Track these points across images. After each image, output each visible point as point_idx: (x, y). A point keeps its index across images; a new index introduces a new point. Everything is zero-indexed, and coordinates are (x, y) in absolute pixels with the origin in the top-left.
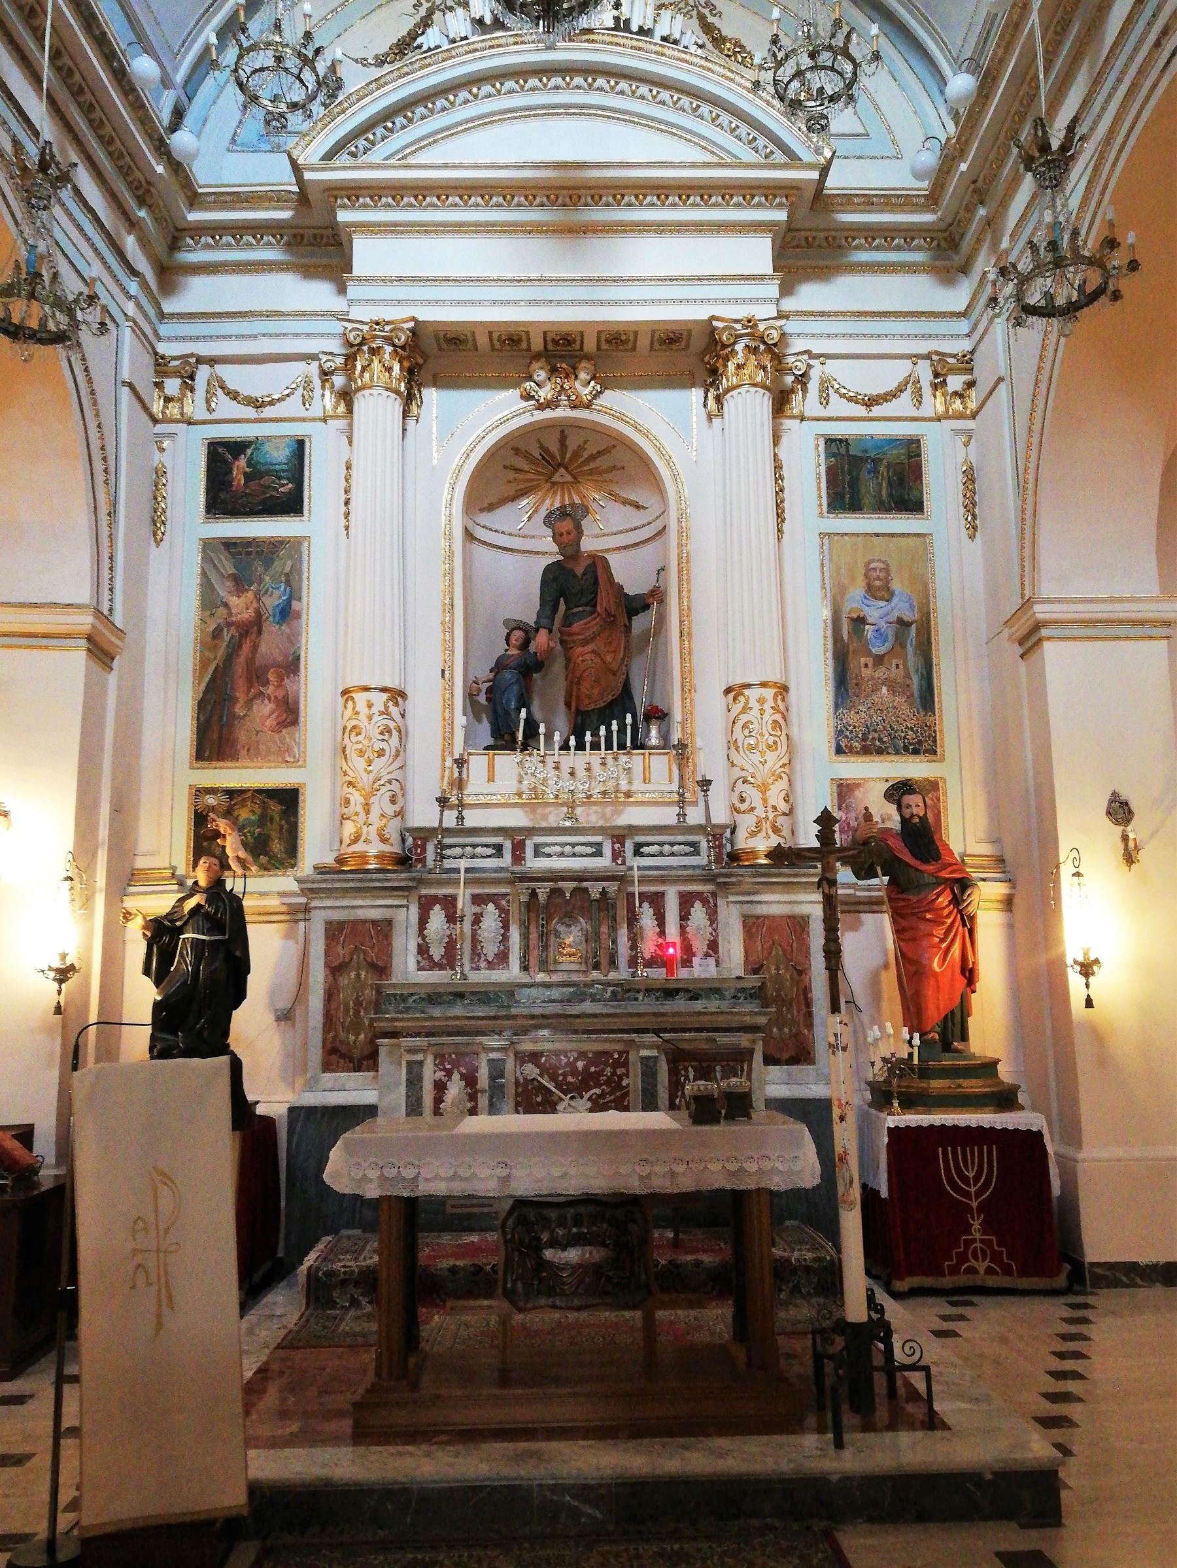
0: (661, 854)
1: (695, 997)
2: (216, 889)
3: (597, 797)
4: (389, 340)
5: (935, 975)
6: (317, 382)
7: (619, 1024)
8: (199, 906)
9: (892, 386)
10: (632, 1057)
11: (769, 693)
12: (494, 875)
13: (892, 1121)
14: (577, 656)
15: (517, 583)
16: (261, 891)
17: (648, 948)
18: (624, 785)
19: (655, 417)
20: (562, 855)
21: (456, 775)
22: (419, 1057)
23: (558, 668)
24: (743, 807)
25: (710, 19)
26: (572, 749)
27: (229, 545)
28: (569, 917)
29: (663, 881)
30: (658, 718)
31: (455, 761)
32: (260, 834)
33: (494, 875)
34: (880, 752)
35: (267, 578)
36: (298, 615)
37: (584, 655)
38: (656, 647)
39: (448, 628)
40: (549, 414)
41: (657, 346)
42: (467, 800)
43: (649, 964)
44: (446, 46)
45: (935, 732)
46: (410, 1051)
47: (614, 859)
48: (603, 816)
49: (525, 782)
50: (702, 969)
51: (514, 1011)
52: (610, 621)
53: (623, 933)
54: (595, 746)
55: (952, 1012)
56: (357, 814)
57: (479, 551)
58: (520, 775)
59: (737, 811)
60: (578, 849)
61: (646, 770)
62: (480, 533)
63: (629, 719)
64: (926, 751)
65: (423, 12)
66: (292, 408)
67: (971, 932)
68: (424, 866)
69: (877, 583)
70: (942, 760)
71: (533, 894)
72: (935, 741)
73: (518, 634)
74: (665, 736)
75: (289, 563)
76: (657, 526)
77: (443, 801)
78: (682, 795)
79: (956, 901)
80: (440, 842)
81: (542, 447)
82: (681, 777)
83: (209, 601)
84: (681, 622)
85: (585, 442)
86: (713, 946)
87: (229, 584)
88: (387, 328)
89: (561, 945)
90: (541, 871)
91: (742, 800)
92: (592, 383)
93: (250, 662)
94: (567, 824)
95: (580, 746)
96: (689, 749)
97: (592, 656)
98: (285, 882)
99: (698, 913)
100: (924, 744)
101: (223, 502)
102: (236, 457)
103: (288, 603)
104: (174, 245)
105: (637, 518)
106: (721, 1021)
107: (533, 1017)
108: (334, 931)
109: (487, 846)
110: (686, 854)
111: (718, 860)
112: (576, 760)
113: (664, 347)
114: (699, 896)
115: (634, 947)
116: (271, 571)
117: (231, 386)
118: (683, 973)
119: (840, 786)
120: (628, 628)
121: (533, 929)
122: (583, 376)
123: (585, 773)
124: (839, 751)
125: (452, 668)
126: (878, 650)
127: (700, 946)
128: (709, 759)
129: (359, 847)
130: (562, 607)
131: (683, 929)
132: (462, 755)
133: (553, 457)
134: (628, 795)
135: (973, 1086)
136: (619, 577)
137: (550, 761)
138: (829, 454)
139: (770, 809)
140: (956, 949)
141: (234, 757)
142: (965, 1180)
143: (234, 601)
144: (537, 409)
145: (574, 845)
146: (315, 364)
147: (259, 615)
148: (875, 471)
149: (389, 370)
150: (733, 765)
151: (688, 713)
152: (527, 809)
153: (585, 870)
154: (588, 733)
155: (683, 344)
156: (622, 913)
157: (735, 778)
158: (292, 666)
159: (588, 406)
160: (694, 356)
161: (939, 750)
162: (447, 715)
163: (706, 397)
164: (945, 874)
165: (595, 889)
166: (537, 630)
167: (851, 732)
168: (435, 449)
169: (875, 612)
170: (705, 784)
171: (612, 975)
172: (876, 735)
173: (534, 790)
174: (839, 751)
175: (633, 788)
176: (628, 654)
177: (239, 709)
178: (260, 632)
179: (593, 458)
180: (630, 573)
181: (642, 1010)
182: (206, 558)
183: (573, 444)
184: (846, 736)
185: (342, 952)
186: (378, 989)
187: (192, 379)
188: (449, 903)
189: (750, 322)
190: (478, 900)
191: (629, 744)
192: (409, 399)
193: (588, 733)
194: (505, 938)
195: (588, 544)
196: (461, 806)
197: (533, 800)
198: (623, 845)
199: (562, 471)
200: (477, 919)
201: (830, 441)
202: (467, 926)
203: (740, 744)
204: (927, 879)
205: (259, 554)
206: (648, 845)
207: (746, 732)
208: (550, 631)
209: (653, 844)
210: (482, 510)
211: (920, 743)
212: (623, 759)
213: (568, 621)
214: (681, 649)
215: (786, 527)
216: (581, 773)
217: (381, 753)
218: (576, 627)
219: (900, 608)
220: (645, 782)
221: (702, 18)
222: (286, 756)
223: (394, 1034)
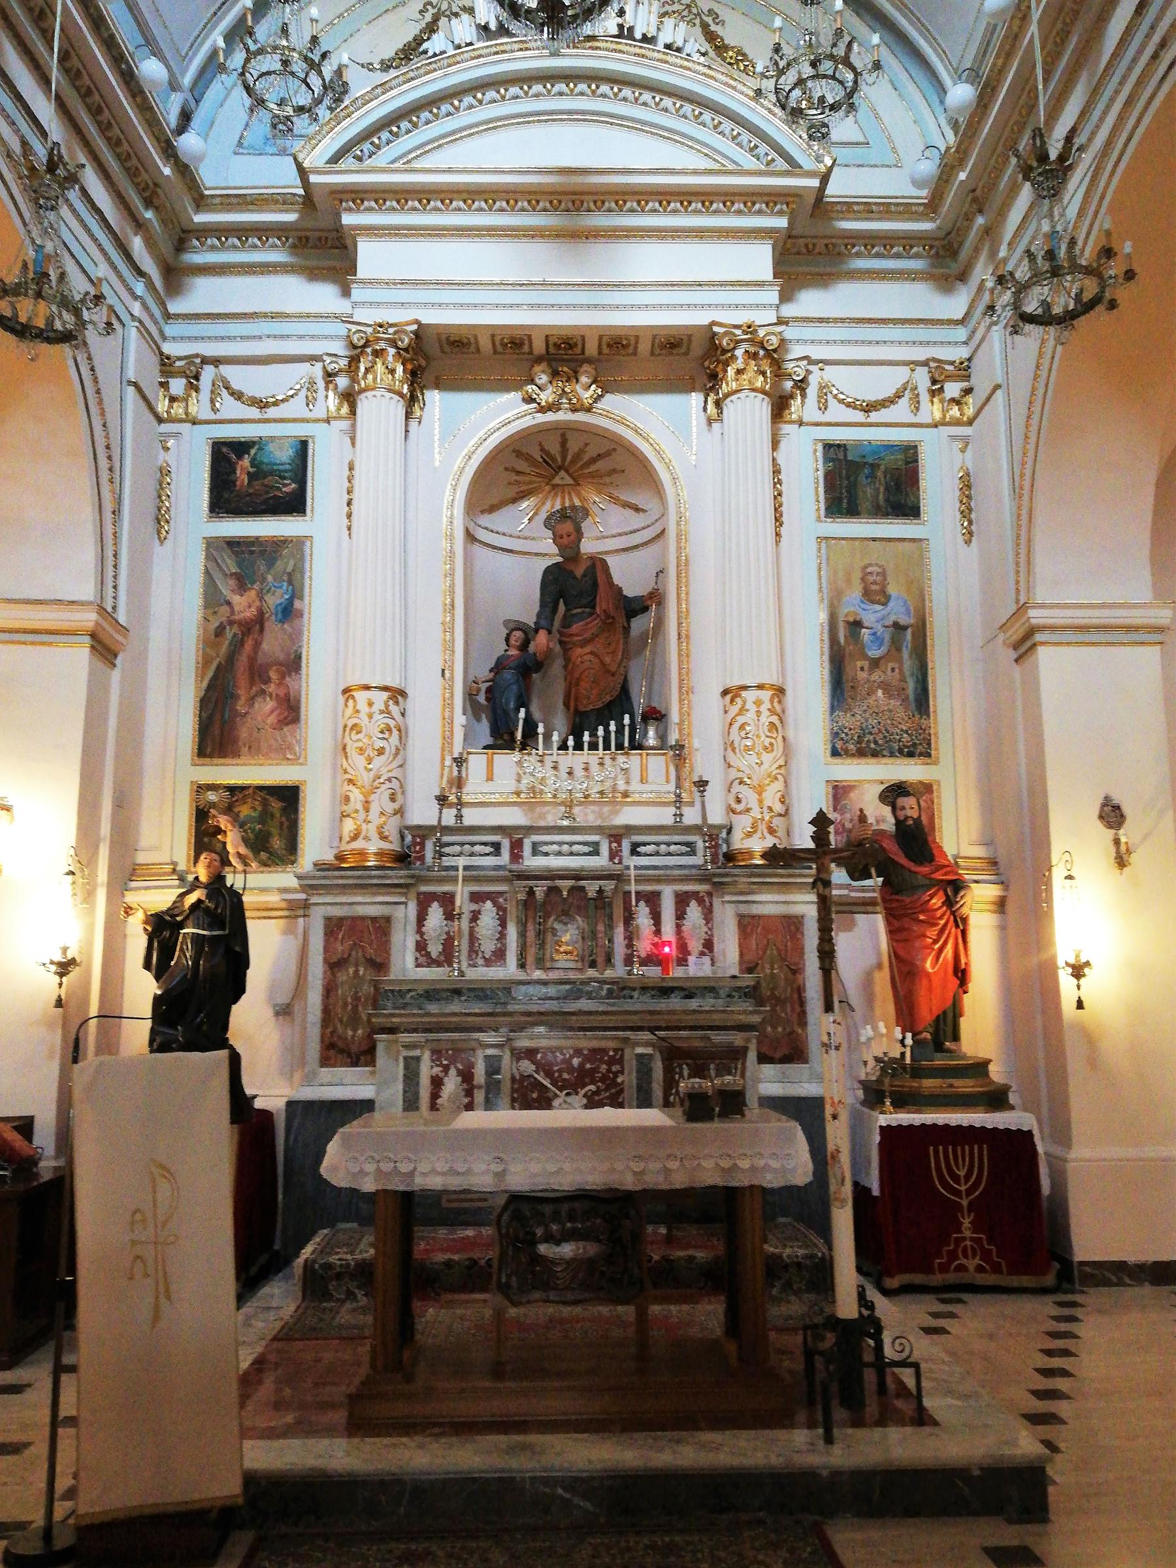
0: (657, 854)
1: (690, 996)
2: (217, 886)
3: (595, 796)
4: (393, 343)
5: (928, 975)
6: (321, 384)
7: (611, 1021)
8: (199, 901)
9: (889, 392)
10: (628, 1053)
11: (766, 695)
13: (883, 1120)
14: (576, 656)
15: (517, 585)
16: (261, 887)
17: (644, 946)
18: (622, 786)
19: (657, 421)
20: (559, 854)
21: (456, 773)
22: (417, 1053)
25: (713, 28)
26: (571, 749)
27: (234, 544)
28: (565, 915)
29: (658, 880)
30: (656, 719)
31: (455, 760)
32: (260, 830)
34: (875, 754)
35: (270, 578)
36: (300, 615)
37: (580, 654)
38: (654, 653)
39: (449, 628)
40: (550, 417)
42: (465, 799)
43: (644, 962)
44: (451, 52)
45: (930, 735)
46: (407, 1047)
47: (611, 858)
50: (697, 968)
51: (510, 1008)
52: (608, 623)
53: (619, 932)
54: (593, 746)
55: (944, 1012)
56: (357, 811)
57: (477, 549)
59: (734, 812)
61: (644, 769)
62: (482, 535)
63: (627, 720)
64: (921, 754)
65: (428, 17)
66: (296, 408)
67: (964, 933)
68: (423, 863)
69: (874, 587)
70: (936, 763)
71: (531, 892)
72: (929, 744)
73: (518, 634)
74: (662, 737)
75: (292, 563)
77: (442, 800)
78: (679, 796)
79: (949, 903)
80: (439, 840)
81: (542, 450)
82: (678, 778)
83: (212, 599)
84: (679, 624)
86: (708, 945)
87: (232, 582)
88: (391, 330)
89: (559, 943)
90: (538, 869)
91: (739, 801)
92: (593, 387)
93: (252, 660)
94: (565, 823)
95: (579, 746)
96: (686, 751)
98: (285, 878)
99: (694, 912)
100: (919, 747)
101: (228, 501)
102: (240, 457)
103: (290, 602)
104: (181, 246)
105: (637, 521)
106: (717, 1019)
107: (529, 1014)
108: (333, 927)
110: (682, 854)
111: (714, 861)
112: (574, 759)
114: (695, 895)
115: (630, 946)
116: (272, 571)
117: (235, 386)
118: (677, 972)
119: (835, 787)
120: (627, 630)
121: (530, 926)
122: (584, 379)
123: (583, 773)
124: (835, 753)
126: (874, 653)
127: (695, 946)
128: (706, 761)
129: (358, 844)
130: (562, 607)
131: (678, 927)
132: (461, 754)
133: (554, 459)
134: (626, 795)
135: (965, 1085)
137: (548, 761)
138: (827, 459)
139: (765, 810)
140: (949, 950)
141: (236, 754)
142: (956, 1179)
143: (236, 599)
145: (571, 844)
146: (319, 365)
147: (261, 612)
148: (872, 476)
149: (392, 372)
150: (729, 766)
151: (685, 715)
153: (582, 869)
154: (586, 733)
156: (618, 912)
158: (293, 664)
159: (589, 410)
160: (694, 361)
161: (933, 752)
163: (706, 402)
164: (939, 876)
165: (592, 888)
166: (536, 631)
167: (847, 734)
168: (437, 450)
169: (871, 616)
170: (702, 784)
171: (609, 973)
172: (871, 738)
173: (532, 789)
174: (835, 753)
175: (631, 788)
176: (627, 656)
177: (241, 707)
178: (262, 630)
179: (593, 460)
180: (630, 576)
181: (638, 1007)
182: (209, 557)
183: (573, 446)
184: (842, 739)
185: (340, 948)
186: (376, 984)
187: (197, 379)
188: (447, 900)
189: (750, 328)
190: (476, 897)
192: (412, 401)
193: (586, 733)
194: (502, 936)
195: (588, 546)
196: (460, 804)
197: (531, 799)
198: (620, 845)
199: (562, 473)
200: (475, 917)
201: (828, 446)
202: (465, 924)
203: (736, 744)
204: (922, 881)
205: (262, 553)
206: (645, 844)
207: (743, 734)
208: (550, 632)
210: (483, 512)
211: (914, 745)
212: (621, 759)
213: (567, 622)
215: (783, 530)
216: (579, 773)
217: (381, 752)
218: (575, 628)
219: (896, 611)
220: (642, 781)
221: (705, 26)
222: (287, 753)
223: (392, 1030)
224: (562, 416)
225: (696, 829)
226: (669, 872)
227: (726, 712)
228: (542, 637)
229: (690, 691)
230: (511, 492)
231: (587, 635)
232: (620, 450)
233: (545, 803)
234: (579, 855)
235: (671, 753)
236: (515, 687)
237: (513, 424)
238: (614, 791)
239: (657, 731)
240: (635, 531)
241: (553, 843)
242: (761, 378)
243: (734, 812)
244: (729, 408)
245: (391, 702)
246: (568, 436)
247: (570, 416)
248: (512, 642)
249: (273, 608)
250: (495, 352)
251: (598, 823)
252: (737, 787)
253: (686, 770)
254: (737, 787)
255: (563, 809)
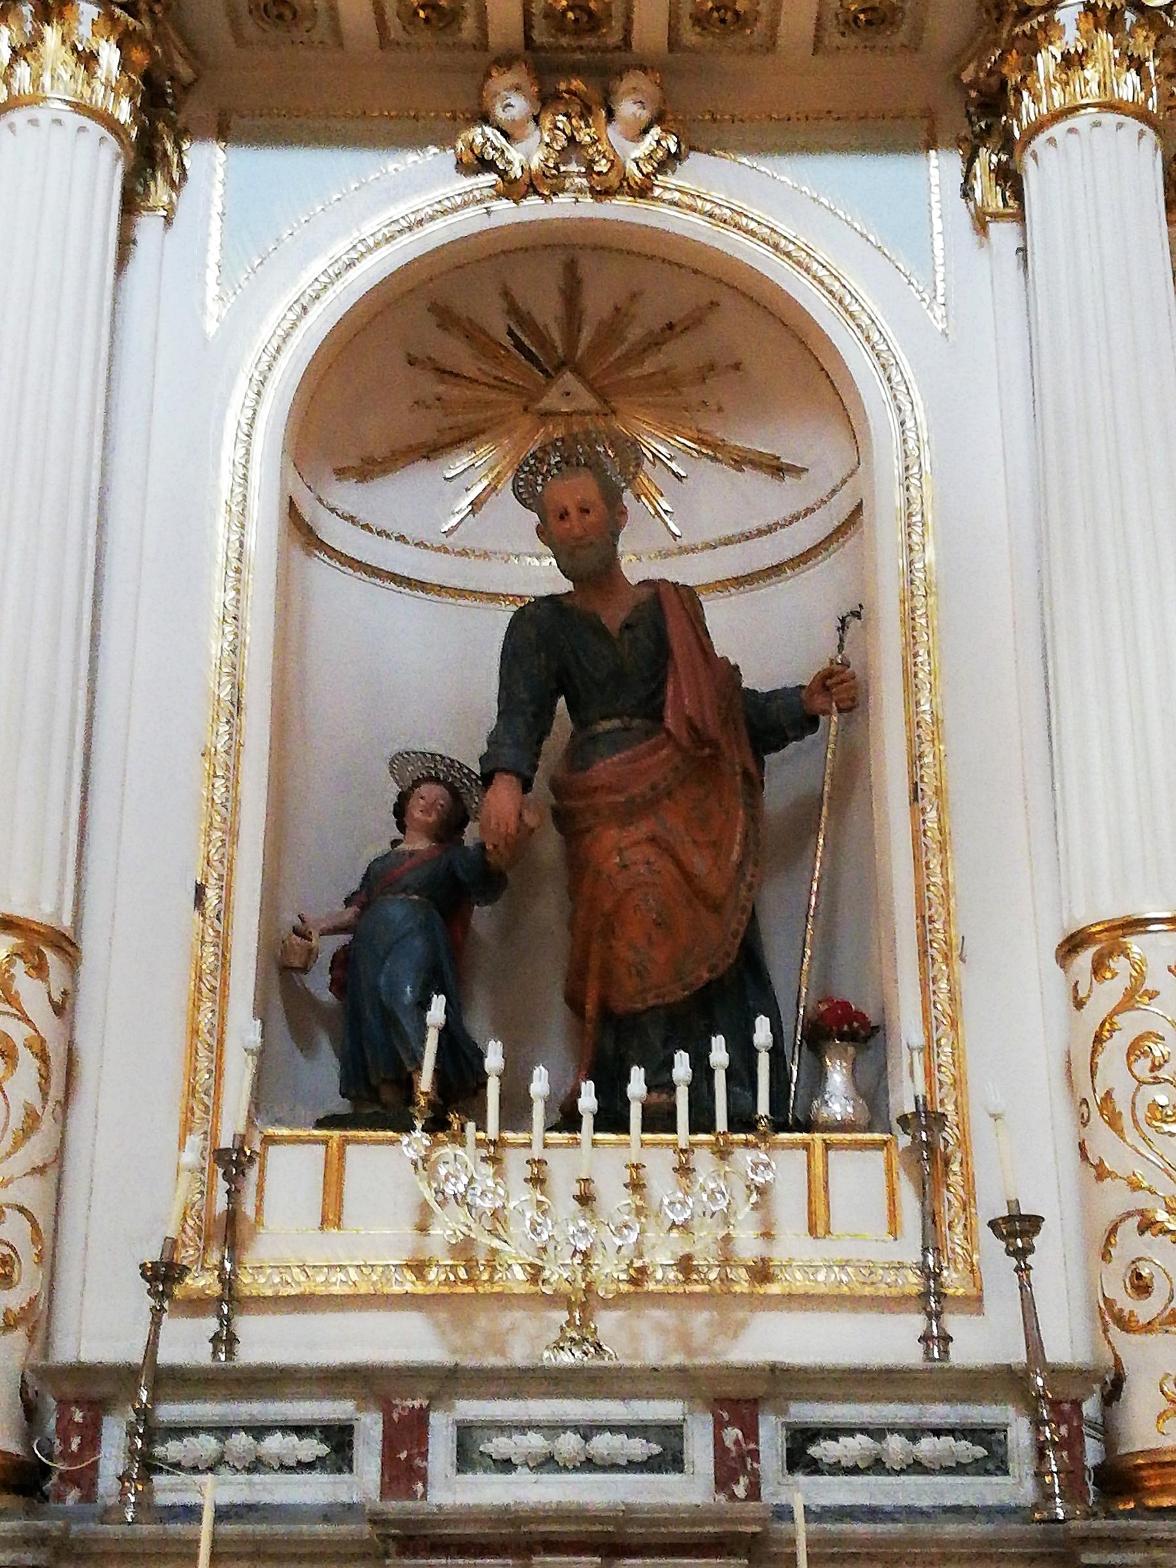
0: (877, 1466)
3: (663, 1276)
12: (321, 1529)
15: (432, 674)
18: (748, 1246)
20: (548, 1463)
21: (221, 1204)
23: (548, 909)
24: (1146, 1309)
26: (588, 1123)
30: (851, 1037)
31: (220, 1156)
33: (321, 1529)
37: (621, 849)
38: (834, 849)
40: (533, 209)
41: (833, 38)
42: (250, 1283)
47: (724, 1480)
48: (685, 1341)
49: (435, 1231)
52: (701, 761)
54: (659, 1119)
57: (322, 575)
58: (425, 1209)
59: (1125, 1323)
60: (603, 1444)
62: (334, 531)
68: (89, 1495)
73: (431, 792)
74: (872, 1094)
76: (840, 508)
77: (163, 1276)
78: (931, 1275)
80: (144, 1414)
81: (513, 310)
82: (931, 1219)
84: (915, 759)
85: (634, 297)
90: (470, 1515)
91: (1141, 1286)
92: (656, 132)
94: (566, 1359)
95: (612, 1118)
96: (950, 1133)
97: (649, 851)
109: (301, 1430)
110: (959, 1469)
112: (600, 1158)
113: (852, 40)
120: (753, 784)
122: (628, 109)
123: (627, 1199)
125: (227, 889)
128: (1019, 1150)
132: (243, 1139)
133: (543, 341)
134: (762, 1272)
136: (580, 1101)
137: (516, 1161)
144: (500, 195)
145: (587, 1431)
149: (88, 59)
150: (1101, 1173)
152: (443, 1316)
153: (627, 1515)
154: (637, 1075)
155: (902, 35)
157: (1113, 1214)
159: (643, 191)
162: (205, 1019)
163: (968, 175)
166: (487, 779)
168: (213, 290)
170: (1018, 1229)
173: (464, 1249)
175: (778, 1254)
179: (654, 342)
180: (762, 640)
183: (597, 302)
191: (763, 1108)
192: (146, 162)
193: (637, 1075)
195: (638, 562)
196: (230, 1300)
197: (462, 1286)
198: (751, 1433)
199: (568, 379)
203: (1122, 1105)
206: (834, 1432)
207: (1142, 1067)
208: (526, 786)
209: (850, 1431)
210: (341, 473)
212: (745, 1158)
213: (580, 752)
214: (918, 834)
216: (614, 1197)
218: (606, 767)
220: (812, 1229)
224: (565, 207)
225: (1007, 1382)
226: (924, 1528)
227: (1079, 1004)
228: (502, 798)
229: (953, 953)
230: (427, 427)
231: (640, 788)
232: (728, 301)
233: (504, 1299)
234: (612, 1467)
235: (905, 1140)
236: (418, 943)
237: (429, 227)
238: (727, 1261)
239: (853, 1072)
240: (770, 529)
241: (523, 1427)
242: (1132, 77)
243: (1125, 1323)
244: (1042, 172)
245: (20, 968)
246: (587, 265)
247: (589, 208)
248: (416, 812)
249: (546, 1443)
250: (384, 41)
251: (676, 1359)
252: (1129, 1242)
253: (952, 1196)
254: (1129, 1242)
255: (562, 1316)
